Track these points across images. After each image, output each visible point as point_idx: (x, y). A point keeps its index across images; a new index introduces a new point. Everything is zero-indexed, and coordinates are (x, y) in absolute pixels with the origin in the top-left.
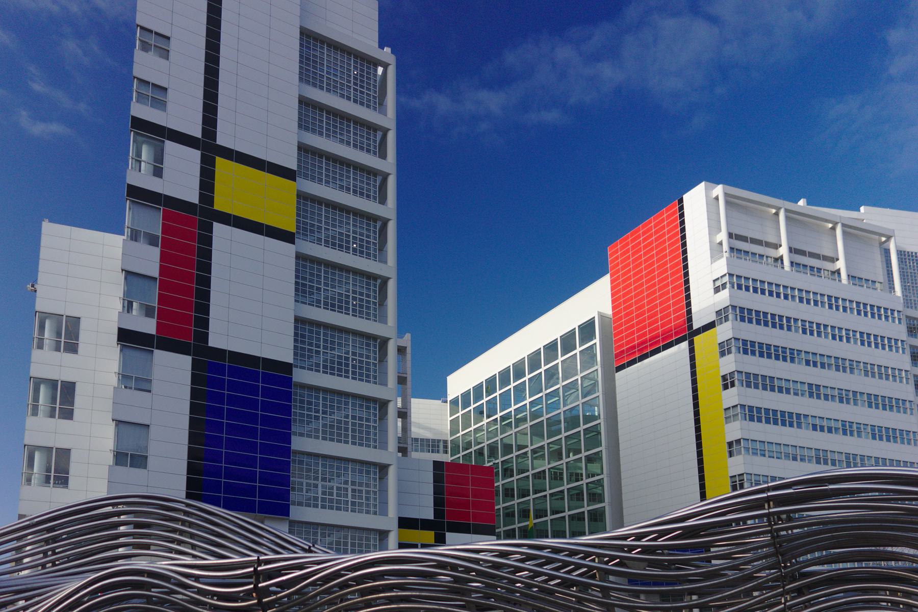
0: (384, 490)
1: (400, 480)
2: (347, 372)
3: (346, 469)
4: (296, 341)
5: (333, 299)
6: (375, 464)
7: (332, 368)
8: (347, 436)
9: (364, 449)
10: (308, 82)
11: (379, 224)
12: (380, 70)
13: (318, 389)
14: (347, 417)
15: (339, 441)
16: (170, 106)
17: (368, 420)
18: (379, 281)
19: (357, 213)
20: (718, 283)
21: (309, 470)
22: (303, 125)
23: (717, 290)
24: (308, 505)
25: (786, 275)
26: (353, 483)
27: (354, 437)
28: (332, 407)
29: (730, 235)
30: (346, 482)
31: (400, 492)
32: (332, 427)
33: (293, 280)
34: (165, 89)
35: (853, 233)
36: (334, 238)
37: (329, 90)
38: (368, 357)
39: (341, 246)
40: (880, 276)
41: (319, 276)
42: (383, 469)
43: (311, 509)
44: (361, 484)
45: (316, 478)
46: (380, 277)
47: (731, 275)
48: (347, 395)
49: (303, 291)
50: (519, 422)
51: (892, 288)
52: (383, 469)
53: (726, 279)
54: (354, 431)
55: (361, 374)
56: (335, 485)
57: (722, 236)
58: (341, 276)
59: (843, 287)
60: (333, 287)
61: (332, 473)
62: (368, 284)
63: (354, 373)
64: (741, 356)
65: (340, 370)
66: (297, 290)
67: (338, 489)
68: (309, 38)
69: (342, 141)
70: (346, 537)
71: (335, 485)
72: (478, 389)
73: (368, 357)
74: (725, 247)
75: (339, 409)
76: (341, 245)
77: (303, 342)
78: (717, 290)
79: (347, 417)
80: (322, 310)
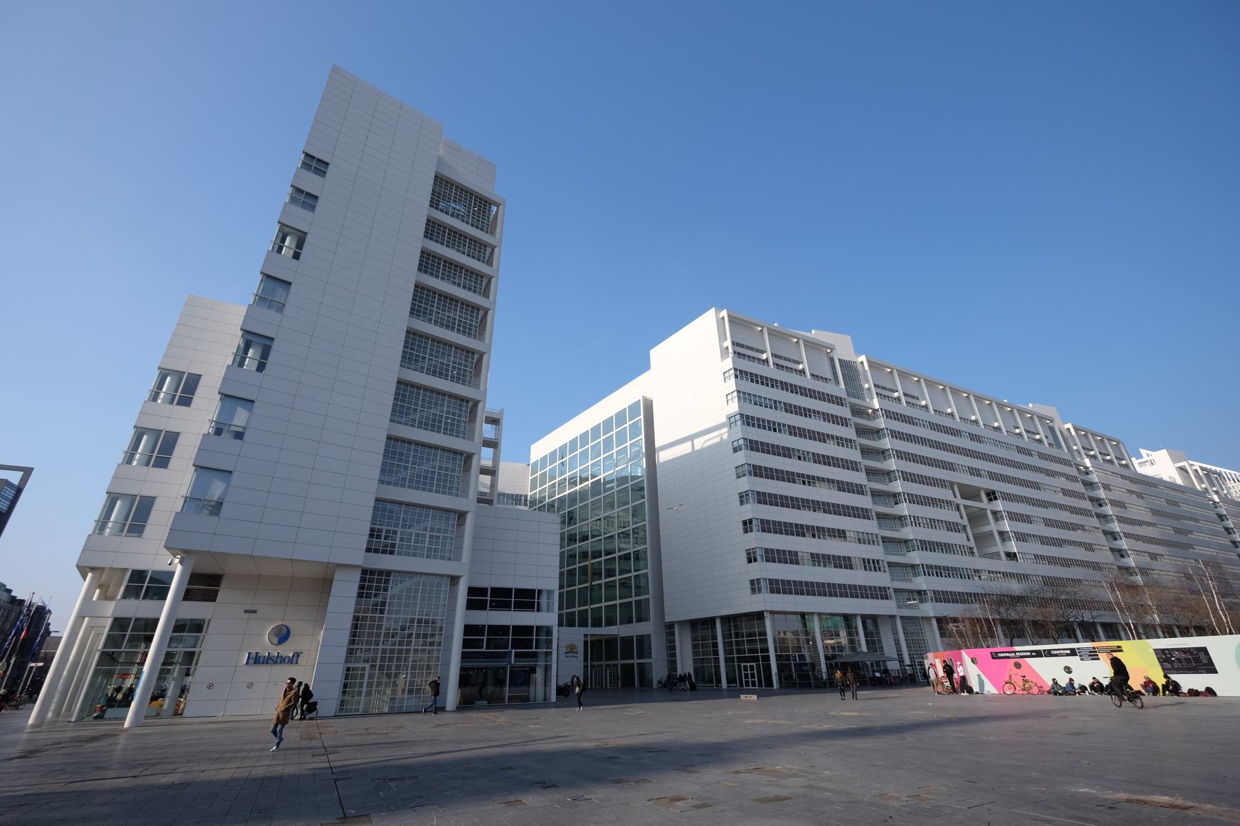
0: (460, 537)
1: (476, 527)
2: (439, 427)
3: (427, 516)
4: (395, 399)
5: (427, 418)
6: (455, 511)
7: (427, 424)
8: (431, 485)
9: (446, 497)
10: (426, 272)
11: (476, 356)
12: (494, 209)
13: (410, 442)
14: (434, 467)
15: (424, 489)
16: (317, 209)
17: (453, 471)
18: (471, 404)
19: (458, 347)
20: (740, 470)
21: (390, 517)
22: (415, 311)
23: (735, 450)
24: (384, 552)
25: (770, 372)
26: (432, 530)
27: (438, 486)
28: (421, 458)
29: (733, 343)
30: (425, 529)
31: (475, 538)
32: (419, 476)
33: (401, 348)
34: (316, 198)
35: (811, 345)
36: (435, 366)
37: (443, 279)
38: (460, 416)
39: (441, 374)
40: (830, 376)
41: (426, 348)
42: (462, 515)
43: (387, 556)
44: (439, 531)
45: (397, 525)
46: (478, 352)
47: (742, 415)
48: (437, 448)
49: (409, 358)
50: (583, 480)
51: (837, 382)
52: (462, 515)
53: (741, 442)
54: (439, 480)
55: (452, 430)
56: (414, 531)
57: (728, 343)
58: (437, 399)
59: (807, 382)
60: (429, 408)
61: (421, 458)
62: (461, 406)
63: (446, 429)
64: (749, 452)
65: (433, 426)
66: (403, 357)
67: (418, 535)
68: (440, 180)
69: (454, 283)
70: (417, 584)
71: (414, 531)
72: (553, 454)
73: (466, 366)
74: (730, 350)
75: (428, 460)
76: (440, 373)
77: (403, 401)
78: (735, 450)
79: (434, 467)
80: (424, 375)
